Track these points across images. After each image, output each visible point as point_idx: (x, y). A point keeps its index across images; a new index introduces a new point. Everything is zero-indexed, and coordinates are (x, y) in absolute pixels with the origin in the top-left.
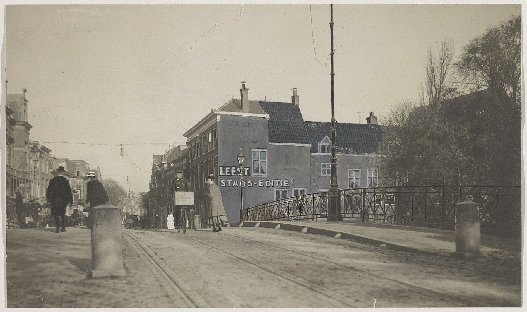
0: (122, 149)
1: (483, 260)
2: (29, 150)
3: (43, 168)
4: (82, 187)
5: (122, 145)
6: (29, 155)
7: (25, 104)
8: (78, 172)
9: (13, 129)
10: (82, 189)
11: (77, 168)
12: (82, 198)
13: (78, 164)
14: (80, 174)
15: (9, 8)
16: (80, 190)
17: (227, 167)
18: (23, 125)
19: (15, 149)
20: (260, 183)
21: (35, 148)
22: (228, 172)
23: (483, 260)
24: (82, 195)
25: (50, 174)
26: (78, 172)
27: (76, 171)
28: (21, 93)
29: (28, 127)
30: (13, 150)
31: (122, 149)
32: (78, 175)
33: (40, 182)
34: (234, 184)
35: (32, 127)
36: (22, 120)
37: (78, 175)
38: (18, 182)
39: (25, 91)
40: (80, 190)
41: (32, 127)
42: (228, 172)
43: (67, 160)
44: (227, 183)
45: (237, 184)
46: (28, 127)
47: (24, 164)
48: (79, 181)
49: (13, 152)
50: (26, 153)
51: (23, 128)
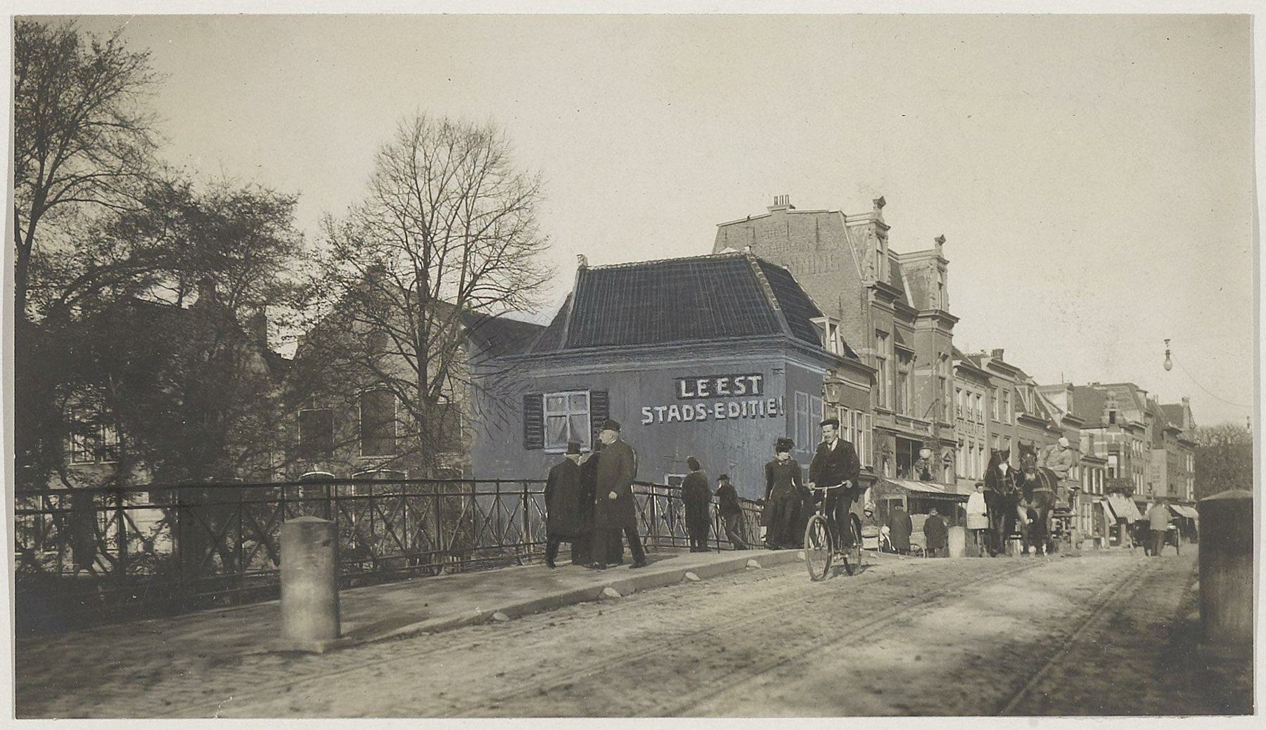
0: (1168, 353)
1: (209, 550)
2: (950, 372)
3: (996, 409)
4: (1122, 448)
5: (1167, 341)
6: (951, 384)
7: (942, 271)
8: (1112, 414)
9: (913, 330)
10: (1122, 454)
11: (1109, 403)
12: (1123, 476)
13: (1111, 393)
14: (1118, 417)
15: (1233, 31)
16: (1118, 456)
17: (700, 378)
18: (934, 318)
19: (917, 373)
20: (717, 410)
21: (971, 371)
22: (703, 391)
23: (209, 550)
24: (1122, 467)
25: (1017, 422)
26: (1112, 414)
27: (1107, 411)
28: (931, 245)
29: (947, 321)
30: (912, 377)
31: (1168, 353)
32: (1112, 420)
33: (985, 443)
34: (671, 414)
35: (957, 319)
36: (933, 305)
37: (1112, 420)
38: (918, 446)
39: (941, 240)
40: (1118, 456)
41: (957, 319)
42: (703, 391)
43: (1071, 387)
44: (655, 414)
45: (677, 414)
46: (947, 321)
47: (937, 405)
48: (1113, 434)
49: (912, 381)
50: (943, 379)
51: (935, 324)
